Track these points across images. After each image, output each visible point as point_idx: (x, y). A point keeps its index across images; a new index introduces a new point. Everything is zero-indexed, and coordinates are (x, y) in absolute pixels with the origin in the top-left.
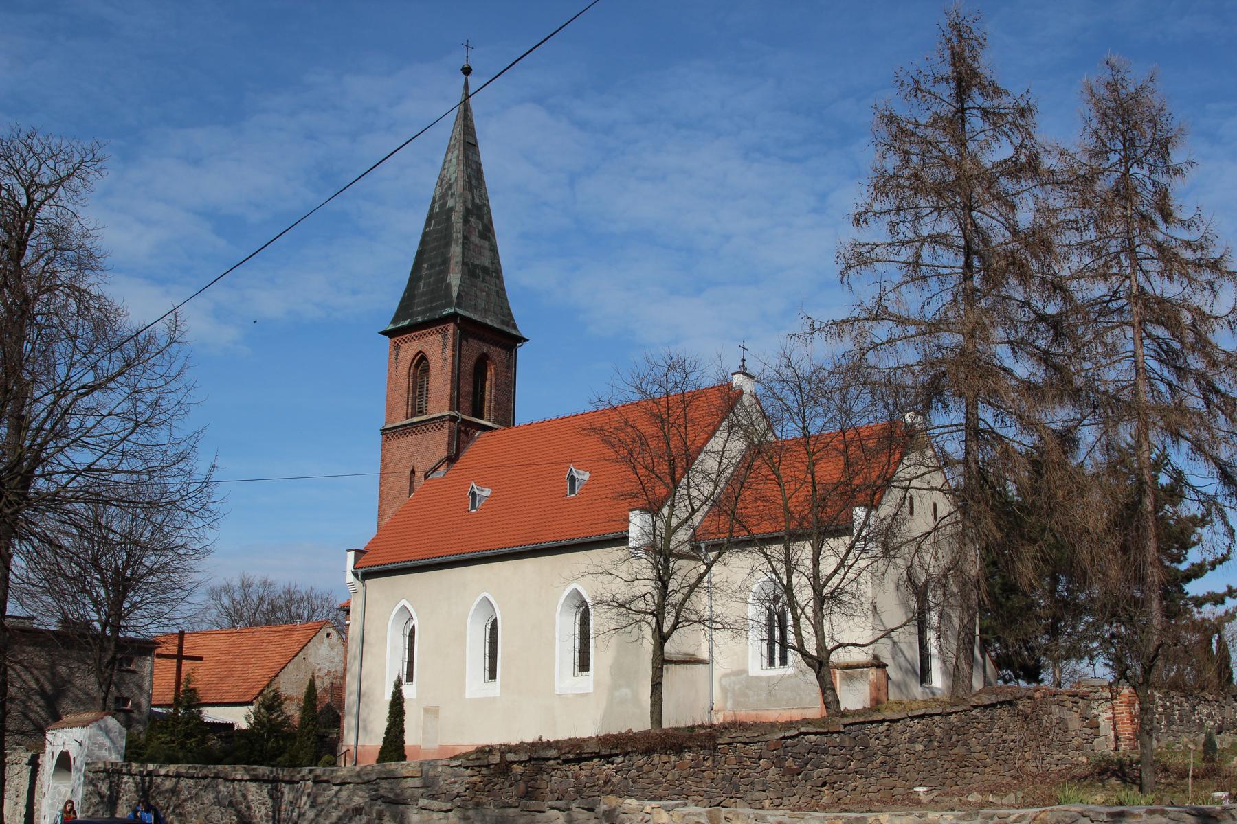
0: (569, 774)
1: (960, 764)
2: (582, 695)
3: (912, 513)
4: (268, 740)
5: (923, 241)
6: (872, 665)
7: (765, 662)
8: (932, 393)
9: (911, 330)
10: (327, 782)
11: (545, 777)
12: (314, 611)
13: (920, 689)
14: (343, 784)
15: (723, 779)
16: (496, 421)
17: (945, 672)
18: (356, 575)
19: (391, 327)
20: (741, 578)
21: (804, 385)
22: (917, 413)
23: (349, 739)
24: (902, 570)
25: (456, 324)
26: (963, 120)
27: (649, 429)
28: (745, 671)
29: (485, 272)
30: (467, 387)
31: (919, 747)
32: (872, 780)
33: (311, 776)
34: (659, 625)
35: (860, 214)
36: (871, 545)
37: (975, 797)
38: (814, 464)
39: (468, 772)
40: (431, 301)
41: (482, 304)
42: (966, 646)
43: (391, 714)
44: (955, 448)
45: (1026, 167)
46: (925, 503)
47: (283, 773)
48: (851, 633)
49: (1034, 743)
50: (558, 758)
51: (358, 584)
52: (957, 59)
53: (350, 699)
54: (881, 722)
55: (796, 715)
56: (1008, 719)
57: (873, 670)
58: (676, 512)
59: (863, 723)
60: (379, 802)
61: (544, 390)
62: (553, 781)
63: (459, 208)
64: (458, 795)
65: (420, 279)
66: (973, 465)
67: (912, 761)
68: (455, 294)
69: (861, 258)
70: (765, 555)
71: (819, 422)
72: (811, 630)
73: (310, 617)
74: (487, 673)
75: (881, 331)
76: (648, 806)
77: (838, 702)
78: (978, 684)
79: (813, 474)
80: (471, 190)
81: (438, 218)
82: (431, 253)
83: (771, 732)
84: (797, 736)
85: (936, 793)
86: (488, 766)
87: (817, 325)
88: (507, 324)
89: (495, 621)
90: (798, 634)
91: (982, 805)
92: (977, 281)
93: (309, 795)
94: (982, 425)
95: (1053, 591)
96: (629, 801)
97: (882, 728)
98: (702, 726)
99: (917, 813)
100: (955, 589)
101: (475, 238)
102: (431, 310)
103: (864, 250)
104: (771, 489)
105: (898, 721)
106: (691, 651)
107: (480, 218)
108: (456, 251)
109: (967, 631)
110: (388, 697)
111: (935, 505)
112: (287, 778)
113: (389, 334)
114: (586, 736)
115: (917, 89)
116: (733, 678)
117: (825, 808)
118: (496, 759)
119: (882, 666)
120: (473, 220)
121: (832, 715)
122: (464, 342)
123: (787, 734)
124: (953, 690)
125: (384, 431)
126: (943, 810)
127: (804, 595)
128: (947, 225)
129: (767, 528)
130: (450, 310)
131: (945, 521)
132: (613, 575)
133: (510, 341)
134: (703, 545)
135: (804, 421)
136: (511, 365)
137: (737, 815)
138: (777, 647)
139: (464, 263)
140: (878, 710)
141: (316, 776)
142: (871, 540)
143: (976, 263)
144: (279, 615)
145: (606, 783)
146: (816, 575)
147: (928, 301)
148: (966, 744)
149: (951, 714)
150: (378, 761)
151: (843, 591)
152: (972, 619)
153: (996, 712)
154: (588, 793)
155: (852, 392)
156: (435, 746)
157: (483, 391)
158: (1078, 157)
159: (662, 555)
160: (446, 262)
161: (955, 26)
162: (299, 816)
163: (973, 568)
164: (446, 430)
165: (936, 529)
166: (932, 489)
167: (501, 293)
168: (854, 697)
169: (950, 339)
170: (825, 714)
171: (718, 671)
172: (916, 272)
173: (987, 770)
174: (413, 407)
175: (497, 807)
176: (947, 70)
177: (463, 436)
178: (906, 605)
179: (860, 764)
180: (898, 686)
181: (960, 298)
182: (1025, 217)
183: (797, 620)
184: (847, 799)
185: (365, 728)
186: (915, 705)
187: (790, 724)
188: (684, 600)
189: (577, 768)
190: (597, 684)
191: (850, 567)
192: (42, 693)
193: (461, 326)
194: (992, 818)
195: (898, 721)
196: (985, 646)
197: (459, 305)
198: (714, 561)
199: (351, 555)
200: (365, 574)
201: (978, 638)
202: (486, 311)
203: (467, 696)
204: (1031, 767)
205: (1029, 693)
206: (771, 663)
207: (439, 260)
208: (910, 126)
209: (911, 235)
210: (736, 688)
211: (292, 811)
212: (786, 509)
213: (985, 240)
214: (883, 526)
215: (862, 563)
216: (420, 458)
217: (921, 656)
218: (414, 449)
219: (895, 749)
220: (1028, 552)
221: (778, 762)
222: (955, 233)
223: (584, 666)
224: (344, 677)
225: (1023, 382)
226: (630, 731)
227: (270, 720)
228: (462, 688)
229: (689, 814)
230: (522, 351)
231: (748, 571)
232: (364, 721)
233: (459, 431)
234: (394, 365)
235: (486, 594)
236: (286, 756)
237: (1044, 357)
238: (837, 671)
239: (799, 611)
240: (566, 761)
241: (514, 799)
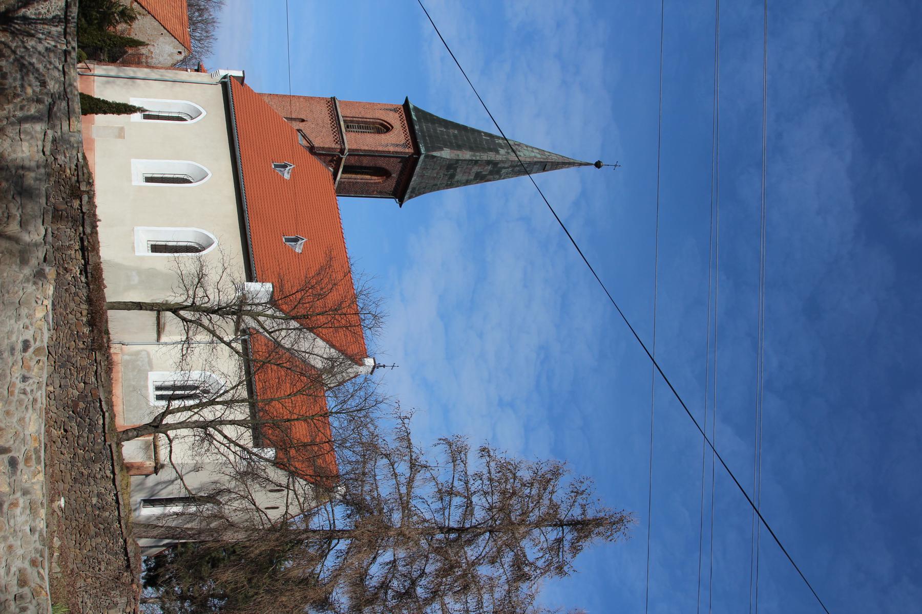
0: (72, 242)
1: (82, 531)
2: (133, 248)
3: (271, 491)
4: (98, 12)
5: (468, 498)
6: (157, 464)
7: (159, 384)
8: (357, 505)
9: (403, 490)
10: (66, 61)
11: (70, 224)
12: (199, 41)
13: (139, 500)
14: (64, 73)
15: (69, 356)
16: (340, 183)
17: (149, 518)
18: (225, 77)
19: (411, 106)
20: (221, 367)
21: (363, 413)
22: (344, 496)
23: (99, 69)
24: (227, 486)
25: (413, 154)
26: (555, 525)
27: (332, 299)
28: (152, 369)
29: (450, 176)
30: (366, 162)
31: (94, 500)
32: (69, 466)
33: (70, 48)
34: (185, 308)
35: (488, 452)
36: (245, 463)
37: (57, 542)
38: (305, 420)
39: (74, 167)
40: (430, 136)
41: (428, 173)
42: (171, 532)
43: (118, 105)
44: (316, 522)
45: (520, 572)
46: (276, 501)
47: (72, 28)
48: (181, 448)
49: (98, 585)
50: (84, 234)
51: (218, 79)
52: (598, 522)
53: (130, 71)
54: (113, 472)
55: (118, 408)
56: (116, 565)
57: (153, 464)
58: (269, 321)
59: (112, 459)
60: (50, 100)
61: (364, 220)
62: (67, 231)
63: (499, 158)
64: (56, 159)
65: (446, 127)
66: (305, 536)
67: (83, 495)
68: (435, 154)
69: (456, 453)
70: (238, 385)
71: (336, 424)
72: (182, 419)
73: (194, 38)
74: (150, 176)
75: (403, 468)
76: (48, 303)
77: (128, 440)
78: (142, 542)
79: (297, 419)
80: (511, 166)
81: (489, 142)
82: (466, 136)
83: (105, 391)
84: (102, 410)
85: (60, 514)
86: (78, 181)
87: (406, 421)
88: (412, 192)
89: (189, 182)
90: (179, 410)
91: (51, 548)
92: (440, 536)
93: (55, 46)
94: (334, 542)
95: (213, 596)
96: (52, 288)
97: (108, 473)
98: (109, 340)
99: (44, 501)
100: (212, 525)
101: (476, 169)
102: (424, 137)
103: (462, 455)
104: (287, 389)
105: (114, 484)
106: (167, 328)
107: (491, 173)
108: (467, 155)
109: (183, 533)
110: (134, 102)
111: (277, 508)
112: (68, 30)
113: (406, 105)
114: (101, 254)
115: (577, 492)
116: (146, 360)
117: (47, 431)
118: (83, 188)
119: (156, 471)
120: (489, 167)
121: (118, 436)
122: (399, 160)
123: (103, 403)
124: (138, 524)
126: (47, 520)
127: (208, 414)
128: (479, 515)
129: (258, 386)
130: (423, 150)
131: (264, 517)
132: (223, 270)
133: (400, 194)
134: (246, 337)
135: (336, 413)
136: (382, 194)
137: (42, 369)
138: (171, 393)
139: (457, 161)
140: (122, 470)
141: (70, 53)
142: (249, 463)
143: (452, 536)
144: (197, 14)
145: (66, 269)
146: (222, 422)
147: (425, 501)
148: (97, 535)
149: (120, 523)
150: (81, 94)
151: (211, 443)
152: (191, 537)
153: (122, 557)
154: (58, 255)
155: (358, 449)
156: (94, 136)
157: (362, 173)
158: (530, 607)
159: (237, 309)
160: (459, 147)
161: (621, 520)
162: (40, 39)
163: (230, 537)
164: (333, 146)
165: (258, 509)
166: (287, 506)
167: (435, 188)
168: (132, 451)
169: (397, 517)
170: (119, 430)
171: (153, 349)
172: (445, 493)
173: (78, 551)
174: (352, 122)
175: (47, 190)
176: (590, 515)
177: (329, 158)
178: (200, 489)
179: (81, 457)
180: (142, 484)
181: (426, 525)
182: (484, 571)
183: (189, 408)
184: (54, 448)
185: (108, 82)
186: (126, 496)
187: (111, 405)
188: (203, 326)
189: (77, 248)
190: (142, 258)
191: (228, 448)
193: (412, 158)
194: (42, 556)
195: (114, 484)
196: (174, 547)
197: (427, 156)
198: (232, 348)
199: (240, 74)
200: (225, 85)
201: (177, 541)
202: (422, 176)
203: (133, 160)
204: (80, 583)
205: (136, 580)
206: (158, 388)
207: (460, 143)
208: (550, 488)
209: (473, 489)
210: (139, 363)
211: (43, 34)
212: (272, 400)
213: (469, 542)
214: (259, 471)
215: (232, 457)
217: (167, 499)
218: (320, 122)
219: (92, 482)
220: (242, 576)
221: (82, 397)
222: (474, 521)
223: (155, 248)
224: (148, 66)
225: (366, 570)
226: (105, 287)
227: (113, 13)
228: (138, 157)
229: (42, 333)
230: (392, 202)
231: (226, 373)
232: (114, 82)
233: (334, 155)
234: (383, 107)
235: (210, 175)
236: (86, 26)
237: (384, 586)
238: (151, 438)
239: (196, 410)
240: (82, 240)
241: (53, 200)
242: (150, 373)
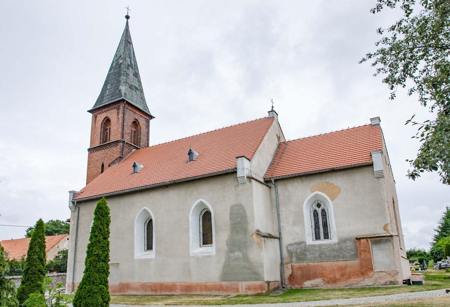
125: (89, 150)
190: (218, 250)
192: (8, 260)
206: (317, 237)
210: (298, 251)
216: (106, 159)
218: (104, 155)
228: (132, 254)
234: (94, 124)
235: (145, 208)
242: (308, 243)
